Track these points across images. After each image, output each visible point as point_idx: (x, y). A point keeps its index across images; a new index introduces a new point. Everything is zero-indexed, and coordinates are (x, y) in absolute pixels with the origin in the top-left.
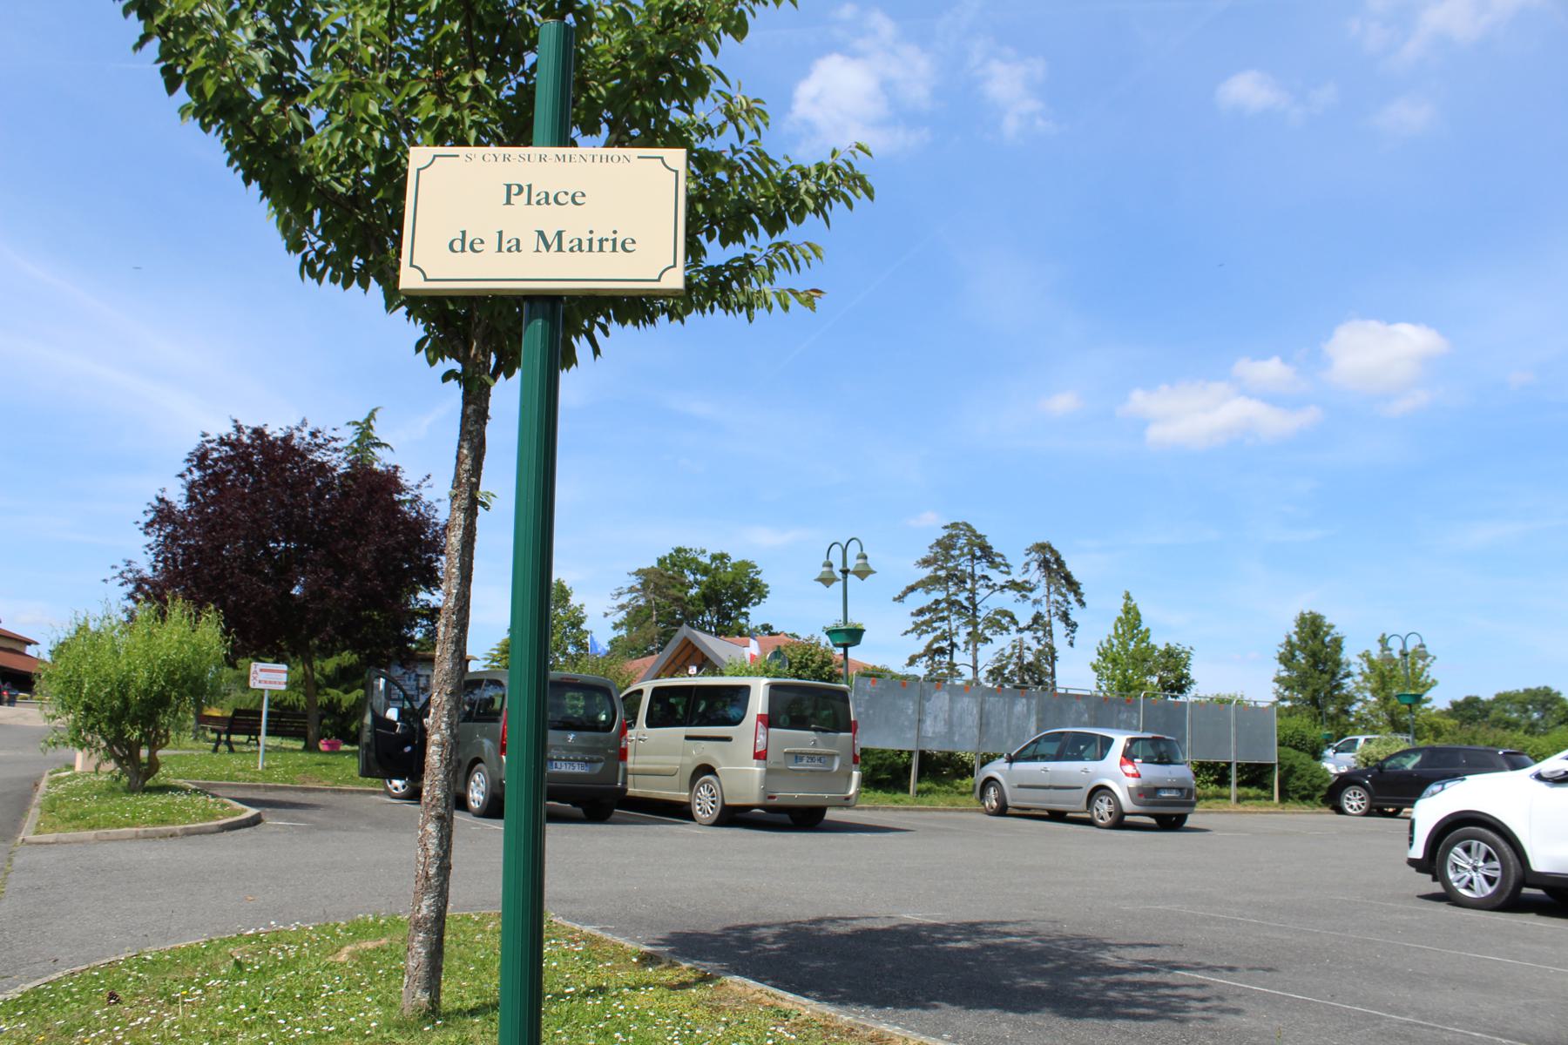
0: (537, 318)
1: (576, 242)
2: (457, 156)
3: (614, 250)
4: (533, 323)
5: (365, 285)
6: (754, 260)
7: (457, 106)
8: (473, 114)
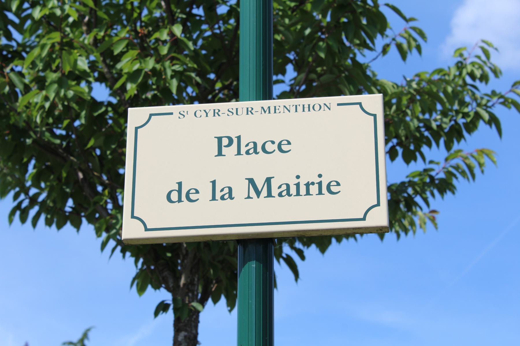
0: (250, 260)
1: (284, 187)
2: (172, 114)
3: (320, 193)
4: (247, 266)
5: (77, 225)
6: (433, 173)
7: (160, 59)
8: (173, 65)
